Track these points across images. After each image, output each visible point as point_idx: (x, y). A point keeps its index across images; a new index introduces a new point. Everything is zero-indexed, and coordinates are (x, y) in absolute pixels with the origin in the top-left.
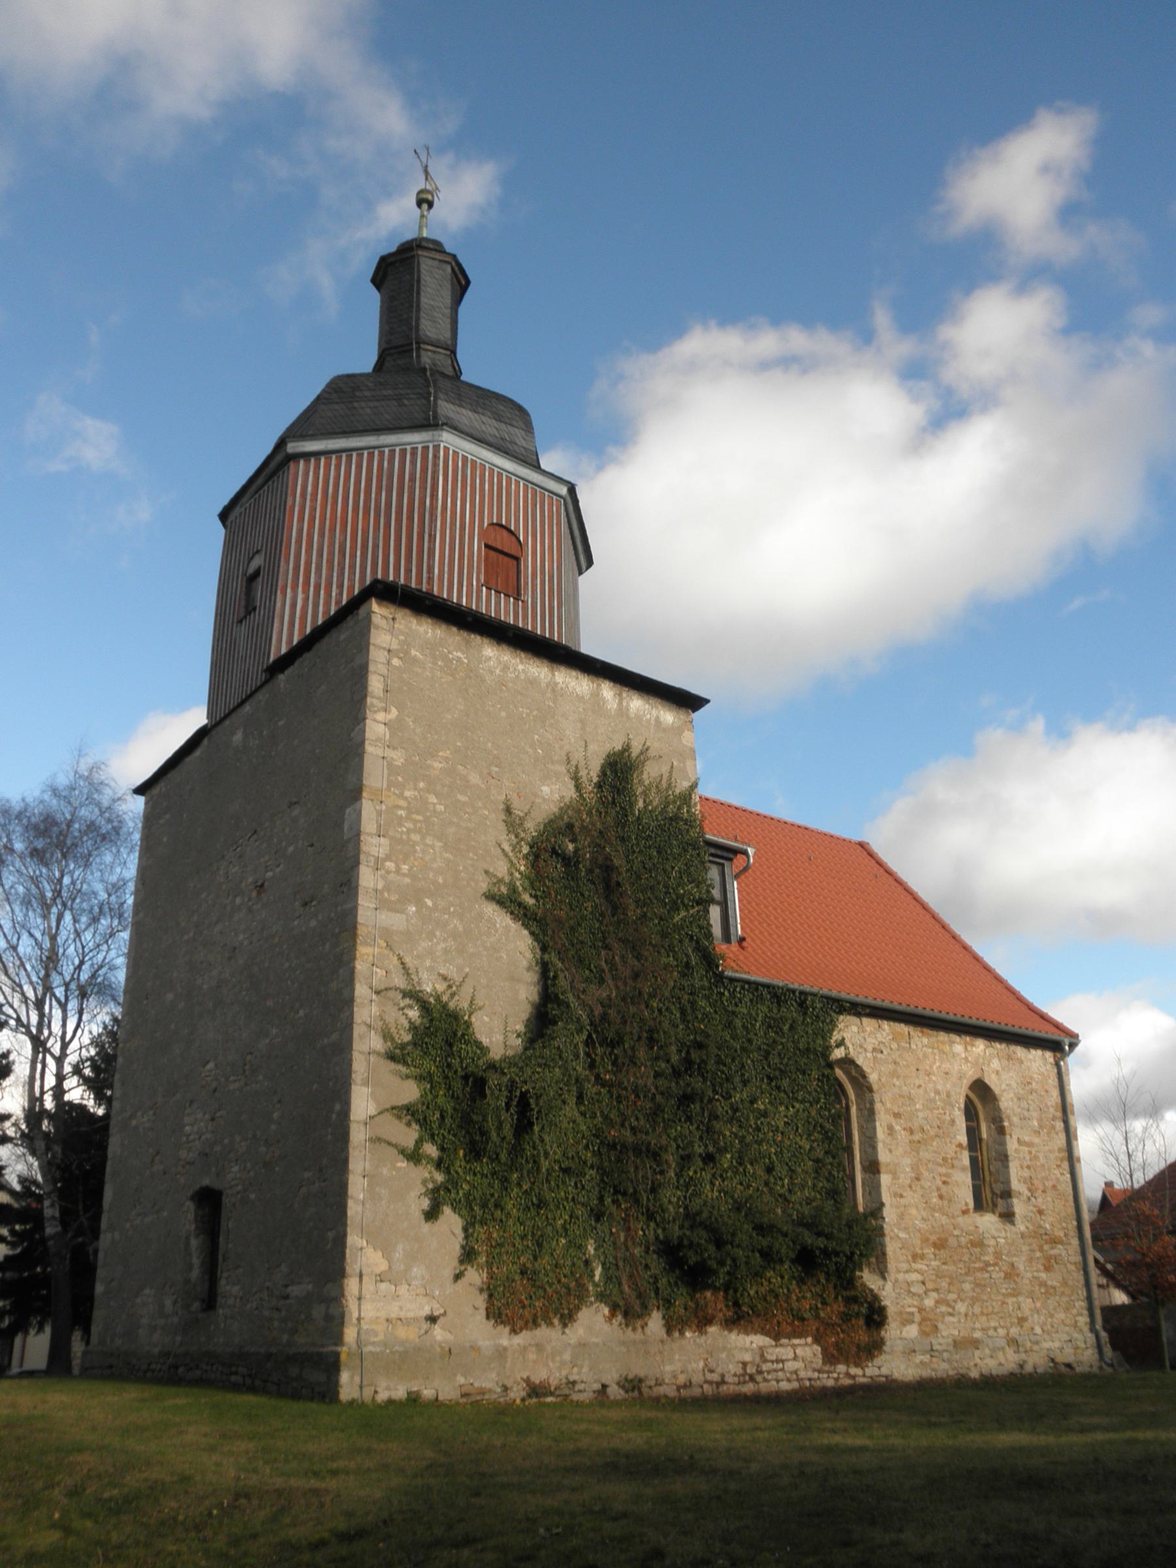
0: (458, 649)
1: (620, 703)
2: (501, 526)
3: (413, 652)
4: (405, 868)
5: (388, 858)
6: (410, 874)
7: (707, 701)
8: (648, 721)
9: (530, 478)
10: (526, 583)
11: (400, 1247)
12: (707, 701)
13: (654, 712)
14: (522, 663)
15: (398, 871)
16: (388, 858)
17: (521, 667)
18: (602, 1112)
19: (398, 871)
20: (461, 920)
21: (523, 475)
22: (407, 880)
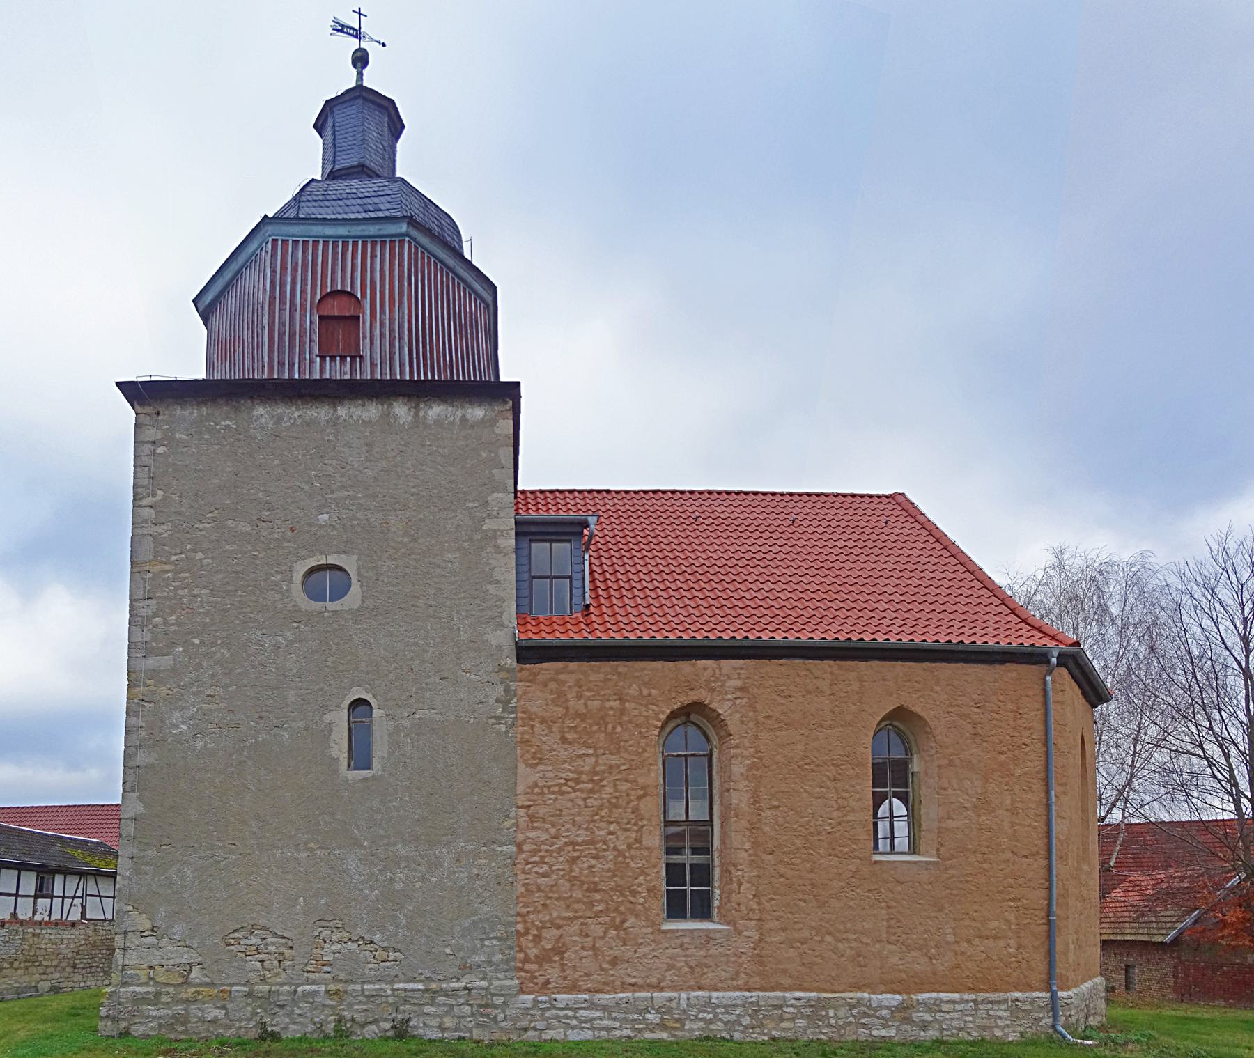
0: (228, 418)
1: (417, 414)
2: (342, 292)
3: (178, 436)
4: (172, 619)
5: (155, 615)
6: (178, 623)
7: (118, 384)
8: (452, 423)
9: (366, 233)
10: (364, 337)
11: (162, 911)
12: (118, 384)
13: (459, 413)
14: (298, 409)
15: (165, 623)
16: (155, 615)
17: (297, 414)
18: (1197, 583)
19: (165, 623)
20: (229, 649)
21: (359, 233)
22: (174, 628)
